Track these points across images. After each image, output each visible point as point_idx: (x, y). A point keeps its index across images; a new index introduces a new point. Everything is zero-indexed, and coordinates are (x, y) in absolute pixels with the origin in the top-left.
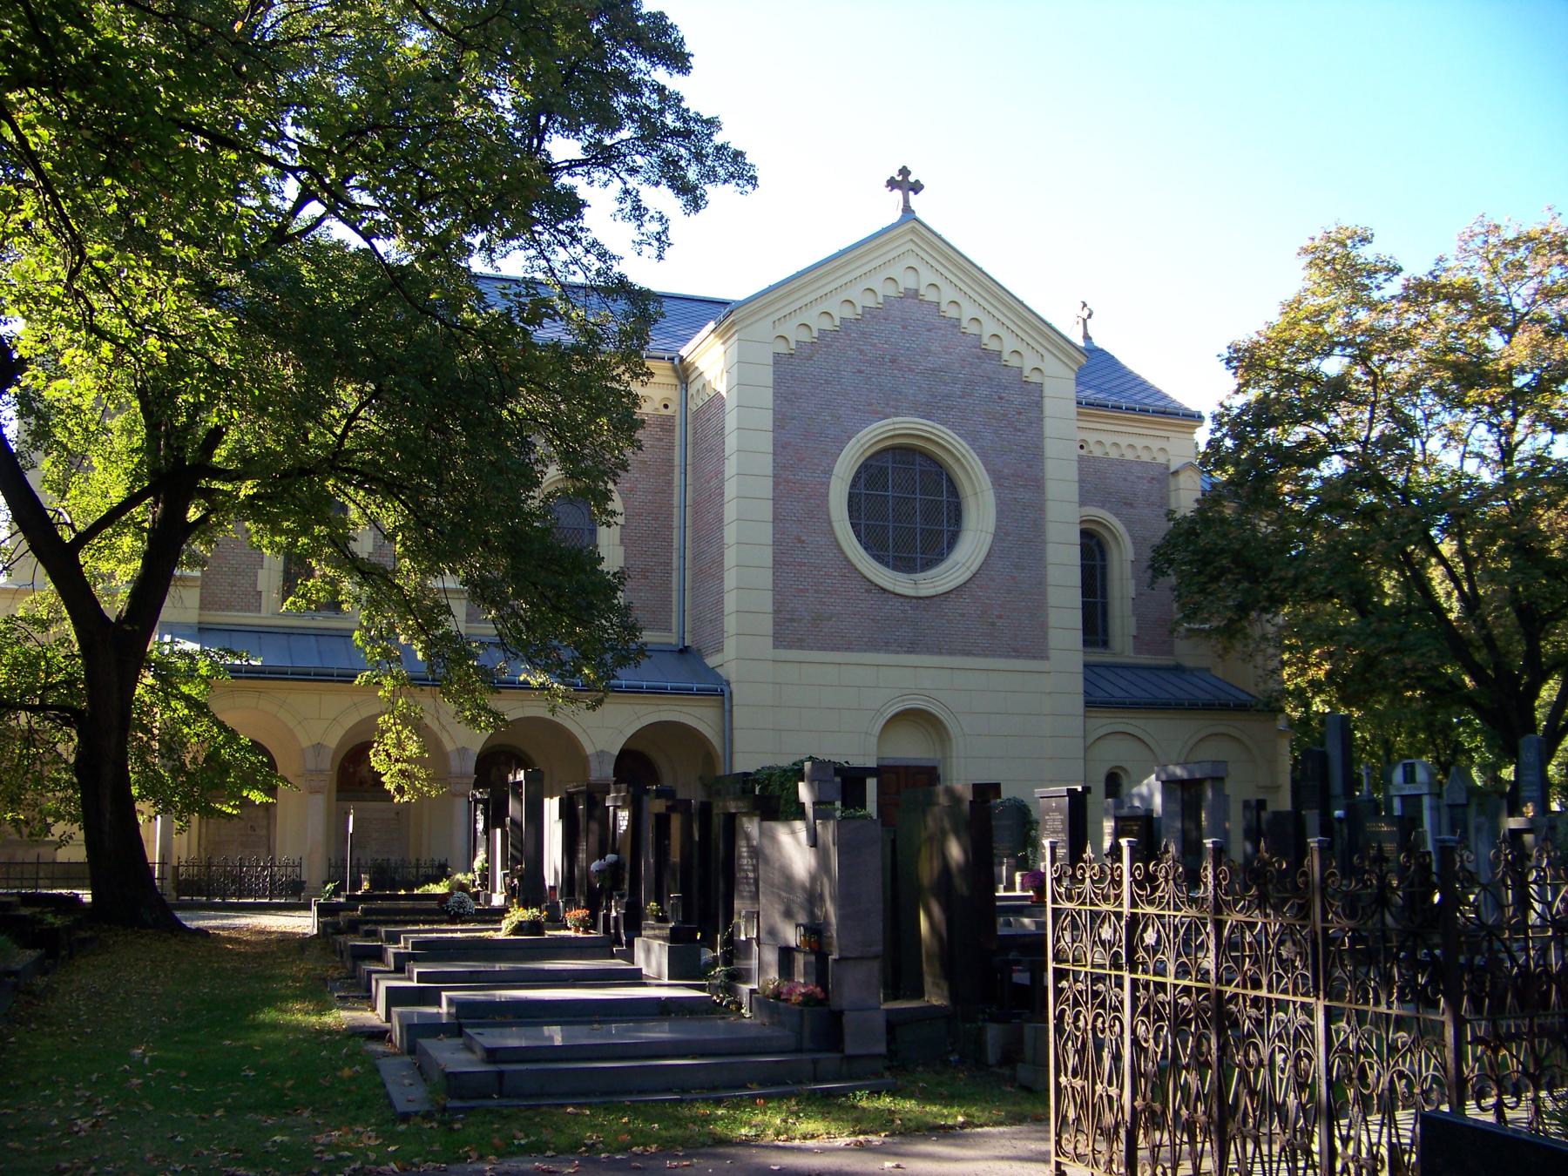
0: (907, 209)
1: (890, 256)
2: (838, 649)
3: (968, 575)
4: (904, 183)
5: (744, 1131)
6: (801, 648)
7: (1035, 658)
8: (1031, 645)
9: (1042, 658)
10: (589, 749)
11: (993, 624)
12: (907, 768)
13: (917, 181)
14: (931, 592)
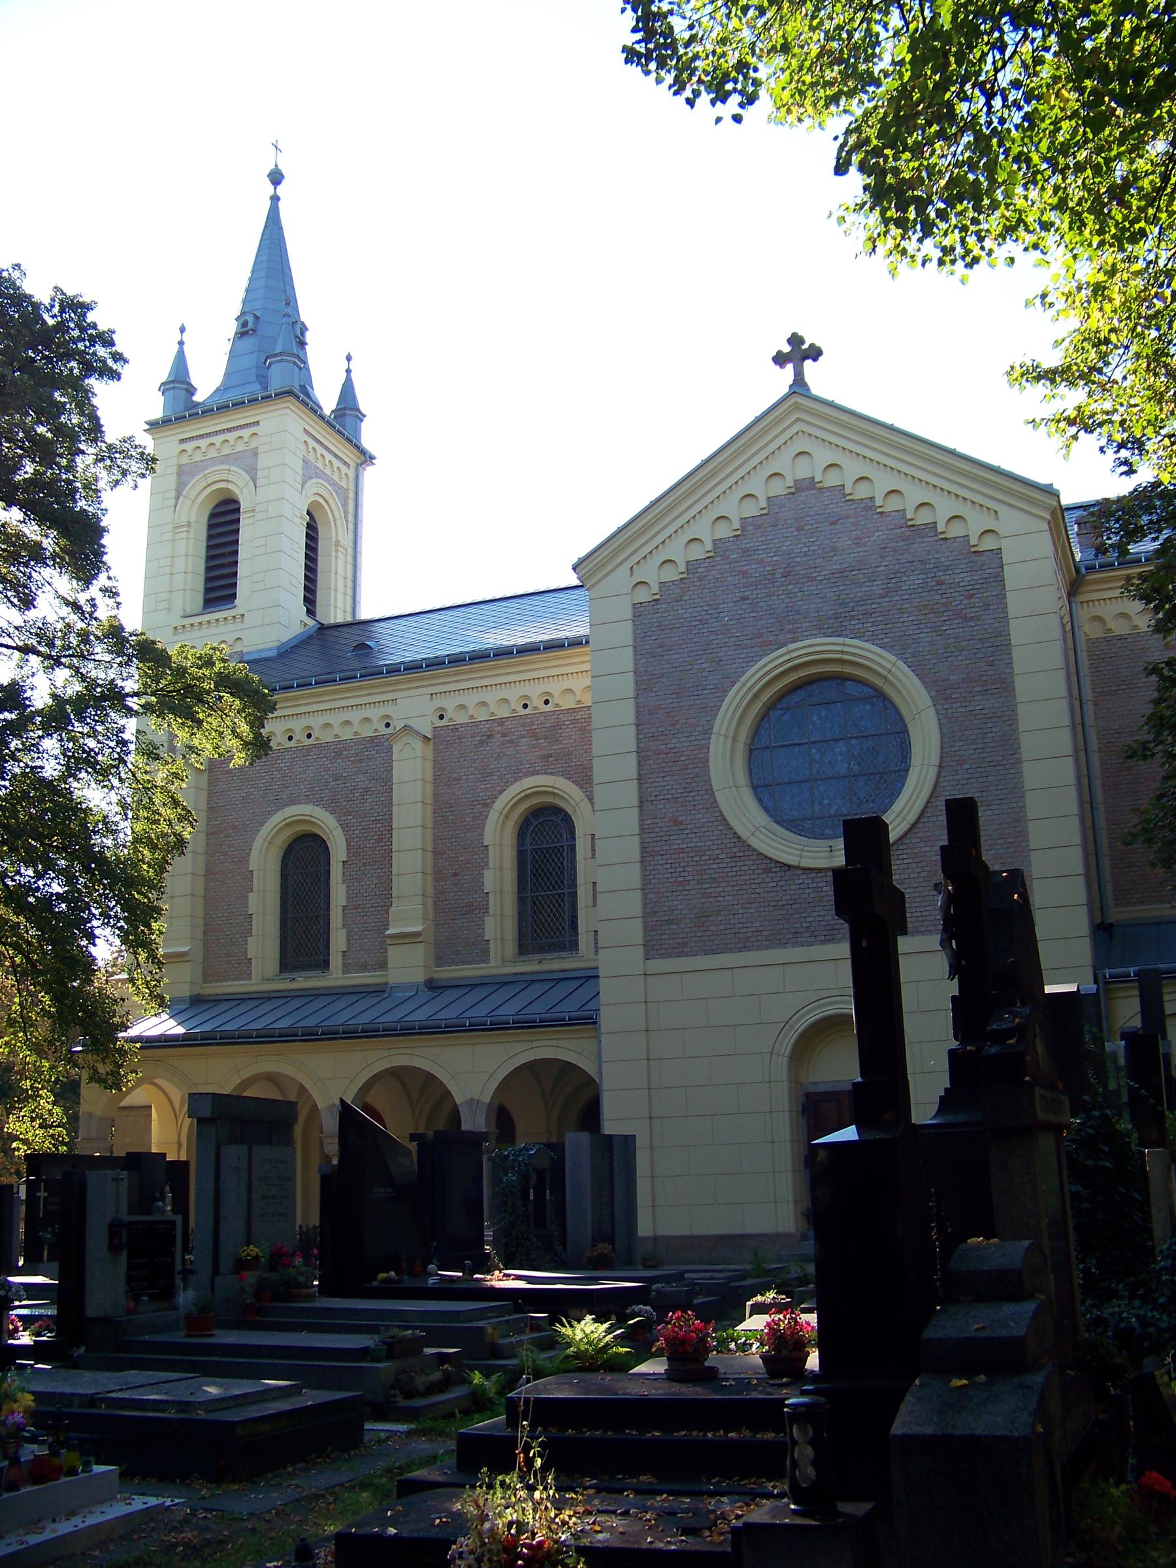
0: (799, 381)
2: (731, 951)
4: (799, 352)
10: (459, 1099)
13: (789, 341)
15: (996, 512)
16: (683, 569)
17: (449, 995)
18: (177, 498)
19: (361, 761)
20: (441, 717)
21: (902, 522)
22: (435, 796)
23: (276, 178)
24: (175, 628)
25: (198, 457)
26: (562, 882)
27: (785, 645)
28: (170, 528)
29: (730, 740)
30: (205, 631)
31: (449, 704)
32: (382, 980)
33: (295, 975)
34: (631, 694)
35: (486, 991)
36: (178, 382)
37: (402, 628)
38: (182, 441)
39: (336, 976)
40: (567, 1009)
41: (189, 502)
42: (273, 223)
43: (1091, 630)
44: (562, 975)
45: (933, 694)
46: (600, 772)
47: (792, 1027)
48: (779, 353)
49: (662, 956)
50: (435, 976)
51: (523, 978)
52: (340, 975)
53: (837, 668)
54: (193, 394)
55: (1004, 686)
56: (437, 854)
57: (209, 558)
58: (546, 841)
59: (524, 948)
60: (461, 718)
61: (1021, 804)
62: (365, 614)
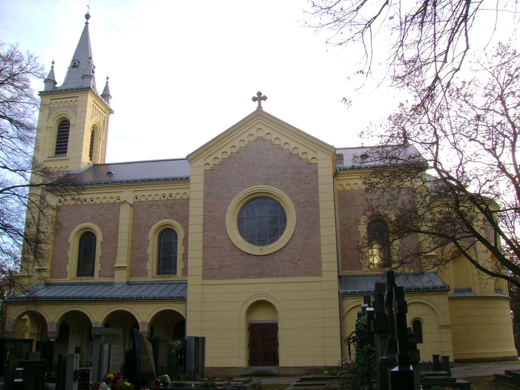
0: (260, 106)
4: (260, 98)
6: (214, 279)
7: (316, 276)
9: (319, 276)
11: (296, 263)
12: (263, 324)
14: (268, 253)
17: (135, 287)
18: (48, 118)
19: (109, 210)
23: (87, 17)
25: (56, 105)
27: (251, 186)
30: (55, 163)
31: (139, 194)
33: (82, 278)
34: (203, 197)
35: (147, 286)
36: (50, 80)
38: (51, 99)
39: (96, 278)
40: (174, 294)
42: (86, 32)
43: (340, 188)
44: (171, 282)
46: (191, 220)
49: (208, 279)
50: (130, 280)
53: (266, 195)
55: (316, 204)
56: (132, 242)
57: (58, 139)
58: (167, 239)
59: (159, 273)
60: (143, 199)
62: (107, 161)
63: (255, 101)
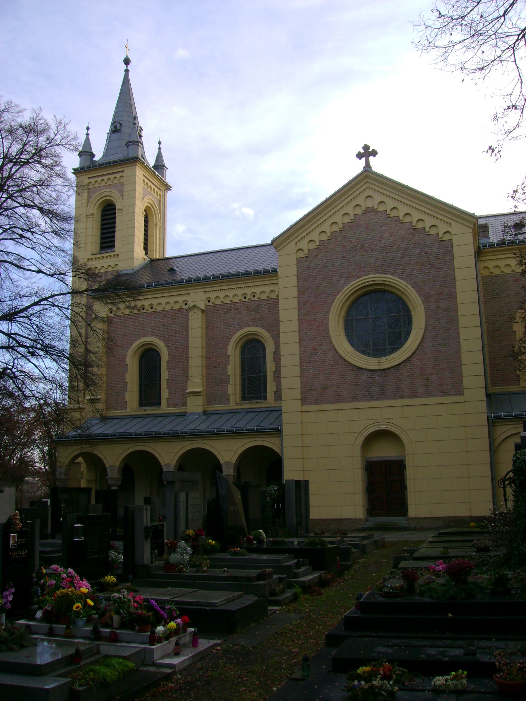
1: (356, 193)
3: (410, 354)
4: (367, 153)
5: (374, 654)
8: (455, 387)
9: (460, 394)
14: (388, 366)
15: (450, 224)
16: (318, 244)
17: (214, 417)
18: (88, 203)
20: (209, 301)
21: (411, 227)
22: (206, 334)
24: (88, 259)
26: (260, 371)
27: (361, 277)
28: (85, 216)
29: (337, 316)
32: (185, 411)
33: (146, 408)
36: (86, 153)
37: (188, 262)
38: (89, 178)
39: (164, 408)
40: (266, 425)
41: (93, 205)
42: (126, 82)
43: (485, 273)
44: (260, 410)
45: (423, 299)
47: (362, 434)
48: (359, 153)
51: (244, 410)
52: (165, 408)
54: (94, 157)
55: (453, 297)
56: (208, 358)
57: (102, 229)
58: (253, 353)
60: (218, 302)
61: (458, 345)
63: (360, 159)
